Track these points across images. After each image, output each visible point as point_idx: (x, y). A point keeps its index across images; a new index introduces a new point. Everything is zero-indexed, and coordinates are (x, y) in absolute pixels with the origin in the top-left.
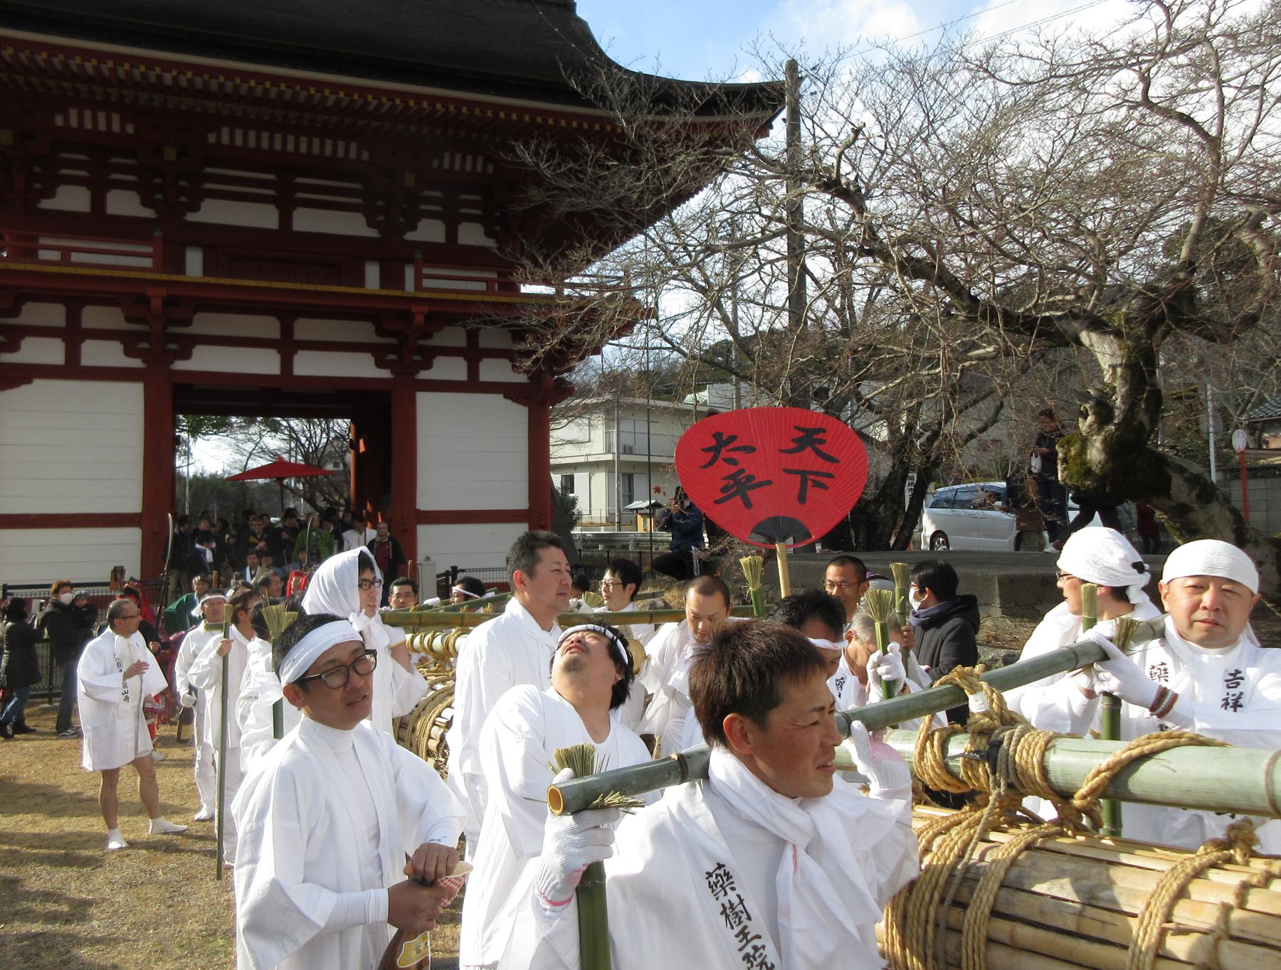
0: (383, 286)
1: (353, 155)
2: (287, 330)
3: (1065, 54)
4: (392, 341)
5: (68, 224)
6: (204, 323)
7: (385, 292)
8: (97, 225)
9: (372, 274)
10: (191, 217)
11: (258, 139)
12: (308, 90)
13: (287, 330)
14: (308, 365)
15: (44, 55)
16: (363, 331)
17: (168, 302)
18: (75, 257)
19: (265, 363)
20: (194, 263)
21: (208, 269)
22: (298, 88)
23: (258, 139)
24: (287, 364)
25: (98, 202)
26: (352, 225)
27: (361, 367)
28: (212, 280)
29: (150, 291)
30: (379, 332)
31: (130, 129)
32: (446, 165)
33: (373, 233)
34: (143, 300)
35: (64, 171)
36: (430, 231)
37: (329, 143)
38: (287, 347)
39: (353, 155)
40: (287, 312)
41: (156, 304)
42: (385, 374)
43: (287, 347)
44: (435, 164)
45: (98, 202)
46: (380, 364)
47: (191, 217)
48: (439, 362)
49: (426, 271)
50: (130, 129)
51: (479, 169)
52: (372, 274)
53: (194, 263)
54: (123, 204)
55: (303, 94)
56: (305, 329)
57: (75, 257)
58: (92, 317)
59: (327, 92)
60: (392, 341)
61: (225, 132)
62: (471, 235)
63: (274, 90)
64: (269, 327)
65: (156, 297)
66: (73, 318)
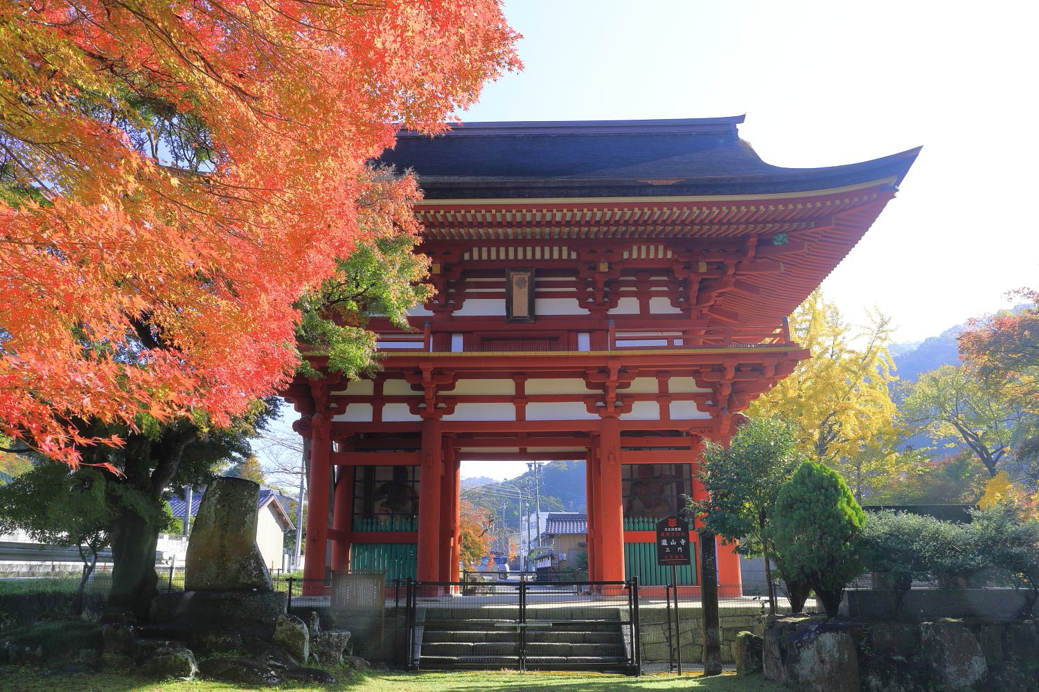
0: (592, 349)
1: (565, 256)
2: (520, 387)
3: (491, 80)
4: (709, 390)
5: (626, 322)
6: (464, 386)
7: (469, 354)
8: (644, 321)
9: (584, 341)
10: (457, 313)
12: (593, 210)
13: (520, 387)
14: (534, 412)
15: (442, 212)
16: (577, 386)
17: (438, 372)
18: (664, 343)
19: (506, 412)
20: (457, 343)
21: (467, 346)
22: (565, 211)
23: (560, 254)
24: (377, 413)
25: (644, 307)
26: (568, 307)
27: (578, 412)
28: (469, 354)
29: (422, 366)
30: (589, 386)
32: (476, 257)
33: (586, 312)
34: (419, 372)
35: (622, 289)
36: (628, 306)
37: (547, 249)
38: (520, 399)
39: (565, 256)
40: (520, 376)
41: (427, 376)
43: (520, 399)
44: (626, 255)
45: (644, 307)
46: (413, 411)
47: (457, 313)
48: (351, 407)
49: (618, 335)
50: (669, 255)
52: (584, 341)
53: (457, 343)
54: (660, 306)
55: (589, 214)
56: (533, 386)
57: (664, 343)
58: (677, 384)
59: (595, 210)
60: (709, 390)
61: (475, 250)
62: (660, 306)
63: (498, 215)
64: (507, 386)
65: (427, 368)
66: (663, 386)
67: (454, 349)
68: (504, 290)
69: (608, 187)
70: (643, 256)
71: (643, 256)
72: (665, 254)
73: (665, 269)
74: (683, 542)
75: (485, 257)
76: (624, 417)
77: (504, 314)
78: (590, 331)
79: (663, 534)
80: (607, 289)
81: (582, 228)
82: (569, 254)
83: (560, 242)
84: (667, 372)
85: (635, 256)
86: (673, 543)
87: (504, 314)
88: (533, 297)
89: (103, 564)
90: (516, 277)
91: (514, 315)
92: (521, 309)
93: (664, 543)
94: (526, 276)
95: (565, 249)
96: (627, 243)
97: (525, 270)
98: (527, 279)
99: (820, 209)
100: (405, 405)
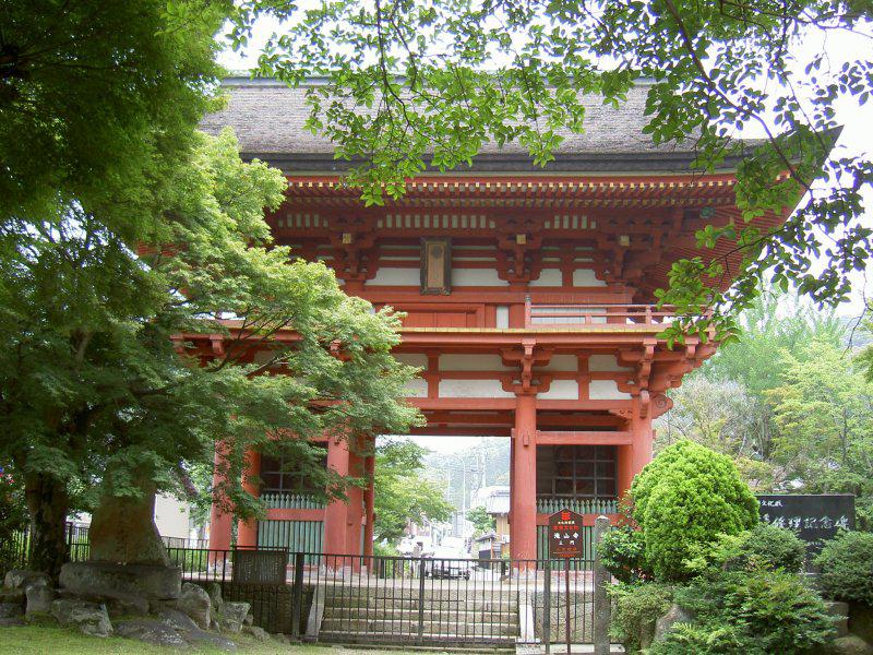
0: (510, 327)
1: (483, 225)
11: (312, 219)
23: (312, 219)
27: (491, 392)
30: (505, 362)
31: (326, 224)
32: (389, 225)
36: (550, 278)
39: (483, 225)
42: (511, 395)
50: (593, 226)
51: (584, 226)
52: (502, 315)
56: (445, 362)
61: (389, 218)
62: (585, 278)
67: (499, 325)
68: (418, 259)
69: (606, 161)
70: (464, 225)
71: (566, 226)
72: (589, 225)
73: (589, 240)
74: (576, 535)
75: (399, 225)
76: (542, 396)
77: (419, 284)
78: (508, 305)
79: (556, 528)
80: (527, 259)
81: (518, 200)
82: (487, 224)
83: (477, 211)
84: (437, 349)
85: (557, 226)
86: (567, 537)
87: (419, 284)
88: (451, 266)
89: (442, 635)
90: (430, 246)
91: (430, 285)
92: (436, 279)
93: (557, 536)
94: (442, 245)
95: (316, 218)
96: (549, 213)
97: (441, 238)
98: (442, 248)
99: (721, 188)
100: (574, 381)
